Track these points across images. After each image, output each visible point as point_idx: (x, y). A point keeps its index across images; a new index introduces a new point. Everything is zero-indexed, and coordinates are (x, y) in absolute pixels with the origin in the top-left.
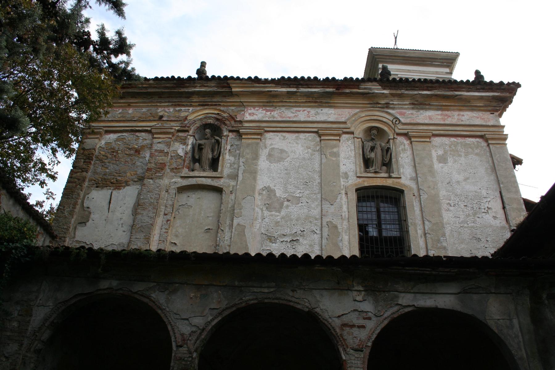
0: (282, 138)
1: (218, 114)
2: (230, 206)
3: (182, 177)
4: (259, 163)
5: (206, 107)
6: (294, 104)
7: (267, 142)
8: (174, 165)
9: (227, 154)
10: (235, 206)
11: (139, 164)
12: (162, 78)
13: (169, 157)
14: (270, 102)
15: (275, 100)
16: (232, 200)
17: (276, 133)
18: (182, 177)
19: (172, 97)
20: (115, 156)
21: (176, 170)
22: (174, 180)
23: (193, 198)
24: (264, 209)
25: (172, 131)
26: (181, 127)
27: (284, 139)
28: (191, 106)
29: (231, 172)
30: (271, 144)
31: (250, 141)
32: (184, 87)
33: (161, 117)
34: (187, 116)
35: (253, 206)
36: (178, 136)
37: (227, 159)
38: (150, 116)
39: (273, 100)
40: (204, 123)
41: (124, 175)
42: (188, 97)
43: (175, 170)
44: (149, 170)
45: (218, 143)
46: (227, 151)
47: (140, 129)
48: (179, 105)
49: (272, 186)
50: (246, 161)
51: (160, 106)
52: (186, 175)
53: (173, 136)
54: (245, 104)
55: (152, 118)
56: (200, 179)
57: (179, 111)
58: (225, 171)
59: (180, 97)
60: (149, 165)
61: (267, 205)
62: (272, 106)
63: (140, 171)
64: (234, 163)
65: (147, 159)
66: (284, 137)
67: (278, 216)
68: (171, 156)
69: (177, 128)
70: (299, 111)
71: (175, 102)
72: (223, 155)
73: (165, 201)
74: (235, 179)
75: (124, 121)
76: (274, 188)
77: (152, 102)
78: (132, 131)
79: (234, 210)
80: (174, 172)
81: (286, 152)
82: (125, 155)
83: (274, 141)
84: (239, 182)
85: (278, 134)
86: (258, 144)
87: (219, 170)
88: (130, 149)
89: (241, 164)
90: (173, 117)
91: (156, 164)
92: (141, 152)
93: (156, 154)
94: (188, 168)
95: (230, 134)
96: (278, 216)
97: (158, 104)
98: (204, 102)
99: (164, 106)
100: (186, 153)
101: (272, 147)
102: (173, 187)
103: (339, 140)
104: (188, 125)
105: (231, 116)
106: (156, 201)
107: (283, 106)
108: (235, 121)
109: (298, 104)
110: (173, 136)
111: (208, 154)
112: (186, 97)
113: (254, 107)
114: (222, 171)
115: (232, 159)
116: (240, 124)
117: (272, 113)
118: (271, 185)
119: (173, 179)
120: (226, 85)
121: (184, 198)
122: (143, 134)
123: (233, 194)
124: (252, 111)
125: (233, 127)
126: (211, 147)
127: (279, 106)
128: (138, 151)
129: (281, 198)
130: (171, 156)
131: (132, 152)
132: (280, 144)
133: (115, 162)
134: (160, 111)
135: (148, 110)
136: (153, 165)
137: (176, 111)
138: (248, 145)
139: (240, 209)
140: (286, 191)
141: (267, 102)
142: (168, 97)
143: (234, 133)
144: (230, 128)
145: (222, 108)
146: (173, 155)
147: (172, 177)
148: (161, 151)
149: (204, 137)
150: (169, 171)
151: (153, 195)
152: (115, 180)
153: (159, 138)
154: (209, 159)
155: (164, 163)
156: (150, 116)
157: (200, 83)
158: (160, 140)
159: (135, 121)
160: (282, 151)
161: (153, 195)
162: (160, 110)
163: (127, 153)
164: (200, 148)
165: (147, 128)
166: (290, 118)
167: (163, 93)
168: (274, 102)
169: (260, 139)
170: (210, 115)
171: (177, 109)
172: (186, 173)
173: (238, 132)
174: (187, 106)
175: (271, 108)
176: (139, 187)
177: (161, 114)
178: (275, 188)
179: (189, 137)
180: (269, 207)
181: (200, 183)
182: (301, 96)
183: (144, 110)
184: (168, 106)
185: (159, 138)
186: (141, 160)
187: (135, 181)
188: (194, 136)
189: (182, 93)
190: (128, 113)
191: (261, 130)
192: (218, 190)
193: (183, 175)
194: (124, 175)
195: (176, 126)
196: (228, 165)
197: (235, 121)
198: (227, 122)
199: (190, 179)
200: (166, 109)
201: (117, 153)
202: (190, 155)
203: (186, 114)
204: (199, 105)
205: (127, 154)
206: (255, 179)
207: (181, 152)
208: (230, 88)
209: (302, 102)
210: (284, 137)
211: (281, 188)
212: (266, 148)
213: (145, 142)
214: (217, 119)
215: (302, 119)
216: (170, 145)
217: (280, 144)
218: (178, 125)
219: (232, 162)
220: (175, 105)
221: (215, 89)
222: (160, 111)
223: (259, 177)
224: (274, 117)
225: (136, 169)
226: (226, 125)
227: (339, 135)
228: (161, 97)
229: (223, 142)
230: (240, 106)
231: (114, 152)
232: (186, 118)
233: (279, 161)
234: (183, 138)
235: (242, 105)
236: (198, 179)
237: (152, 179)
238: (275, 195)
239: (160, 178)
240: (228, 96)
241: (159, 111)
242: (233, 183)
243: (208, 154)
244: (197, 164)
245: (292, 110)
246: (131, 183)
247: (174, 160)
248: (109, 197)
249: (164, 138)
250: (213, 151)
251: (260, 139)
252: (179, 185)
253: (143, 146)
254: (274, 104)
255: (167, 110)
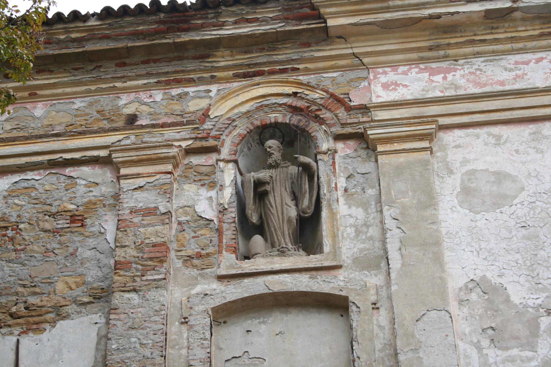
0: (492, 140)
1: (295, 94)
2: (378, 345)
3: (221, 278)
4: (441, 217)
5: (257, 79)
6: (508, 46)
7: (450, 157)
8: (192, 248)
9: (342, 200)
10: (399, 343)
11: (88, 254)
12: (125, 9)
13: (175, 226)
14: (438, 47)
15: (453, 41)
16: (381, 328)
17: (470, 131)
18: (221, 278)
19: (155, 61)
20: (12, 239)
21: (198, 260)
22: (198, 289)
23: (262, 335)
24: (485, 343)
25: (173, 151)
26: (196, 139)
27: (497, 144)
28: (213, 80)
29: (361, 250)
30: (465, 162)
31: (402, 158)
32: (187, 30)
33: (132, 119)
34: (208, 109)
35: (450, 338)
36: (189, 167)
37: (345, 219)
38: (98, 120)
39: (447, 41)
40: (258, 123)
41: (47, 289)
42: (203, 57)
43: (195, 261)
44: (118, 266)
45: (309, 172)
46: (340, 192)
47: (77, 155)
48: (179, 82)
49: (492, 275)
50: (402, 214)
51: (125, 90)
52: (233, 272)
53: (176, 166)
54: (366, 60)
55: (105, 124)
56: (276, 277)
57: (180, 96)
58: (344, 250)
59: (180, 58)
60: (120, 252)
61: (490, 332)
62: (446, 57)
63: (93, 274)
64: (366, 225)
65: (110, 237)
66: (498, 138)
67: (530, 359)
68: (180, 223)
69: (184, 144)
70: (527, 63)
71: (167, 73)
72: (329, 206)
73: (184, 352)
74: (378, 267)
75: (27, 138)
76: (499, 280)
77: (99, 80)
78: (53, 164)
79: (396, 354)
80: (194, 266)
81: (514, 179)
82: (43, 234)
83: (468, 151)
84: (393, 276)
85: (478, 131)
86: (426, 163)
87: (327, 248)
88: (52, 215)
89: (390, 223)
90: (166, 114)
91: (139, 248)
92: (88, 222)
93: (136, 220)
94: (235, 250)
95: (340, 146)
96: (530, 359)
97: (118, 85)
98: (249, 66)
99: (136, 89)
100: (223, 211)
101: (470, 167)
102: (201, 308)
103: (430, 149)
104: (213, 133)
105: (332, 95)
106: (157, 353)
107: (477, 54)
108: (349, 109)
109: (520, 45)
110: (176, 166)
111: (284, 209)
112: (195, 58)
113: (394, 65)
114: (335, 251)
115: (359, 213)
116: (363, 114)
117: (450, 77)
118: (489, 275)
119: (195, 285)
120: (307, 10)
121: (235, 338)
122: (86, 170)
123: (382, 311)
124: (391, 76)
125: (343, 125)
126: (288, 186)
127: (465, 56)
128: (77, 219)
129: (526, 306)
130: (180, 223)
131: (62, 223)
132: (488, 158)
133: (13, 255)
134: (127, 104)
135: (91, 104)
136: (132, 252)
137: (172, 98)
138: (399, 170)
139: (415, 350)
140: (537, 286)
141: (430, 49)
142: (144, 62)
143: (351, 143)
144: (337, 130)
145: (303, 79)
146: (183, 219)
147: (194, 282)
148: (150, 212)
149: (263, 161)
150: (179, 264)
151: (146, 336)
152: (22, 306)
153: (138, 176)
154: (289, 221)
155: (164, 244)
156: (98, 120)
157: (233, 14)
158: (141, 182)
159: (57, 135)
160: (500, 177)
161: (146, 336)
162: (124, 99)
163: (48, 226)
164: (261, 192)
165: (95, 153)
166: (502, 83)
167: (129, 49)
168: (449, 44)
169: (430, 149)
170: (273, 100)
171: (175, 92)
172: (231, 267)
173: (360, 137)
174: (201, 81)
175: (444, 65)
176: (96, 318)
177: (129, 110)
178: (503, 281)
179: (221, 164)
180: (496, 336)
181: (277, 288)
182: (523, 19)
183: (79, 103)
184: (146, 87)
185: (138, 176)
186: (91, 242)
187: (84, 304)
188: (236, 162)
189: (183, 46)
190: (34, 118)
191: (425, 127)
192: (336, 305)
193: (224, 272)
194: (47, 289)
195: (181, 138)
196: (351, 231)
197: (349, 109)
198: (326, 115)
199: (246, 280)
200: (143, 96)
201: (16, 228)
202: (233, 214)
203: (203, 103)
204: (237, 76)
205: (46, 231)
206: (438, 260)
207: (206, 210)
208: (320, 17)
209: (532, 38)
210: (498, 138)
211: (522, 280)
212: (451, 172)
213: (96, 192)
214: (295, 110)
215: (540, 84)
216: (171, 193)
217: (488, 158)
218: (184, 134)
219: (360, 222)
220: (168, 83)
221: (279, 26)
222: (127, 104)
223: (447, 255)
224: (457, 87)
225: (80, 270)
226: (321, 121)
227: (428, 136)
228: (124, 64)
229: (323, 170)
230: (351, 68)
231: (6, 228)
232: (206, 115)
233: (496, 205)
234: (203, 169)
235: (358, 62)
236: (270, 278)
237: (135, 290)
238: (507, 300)
239: (159, 284)
240: (317, 43)
241: (122, 102)
242: (375, 280)
243: (284, 209)
244: (258, 239)
245: (503, 63)
246: (72, 308)
247: (188, 234)
248: (12, 357)
249: (150, 175)
250: (296, 198)
251: (430, 149)
252: (218, 302)
253: (90, 202)
254: (451, 52)
255: (144, 99)
